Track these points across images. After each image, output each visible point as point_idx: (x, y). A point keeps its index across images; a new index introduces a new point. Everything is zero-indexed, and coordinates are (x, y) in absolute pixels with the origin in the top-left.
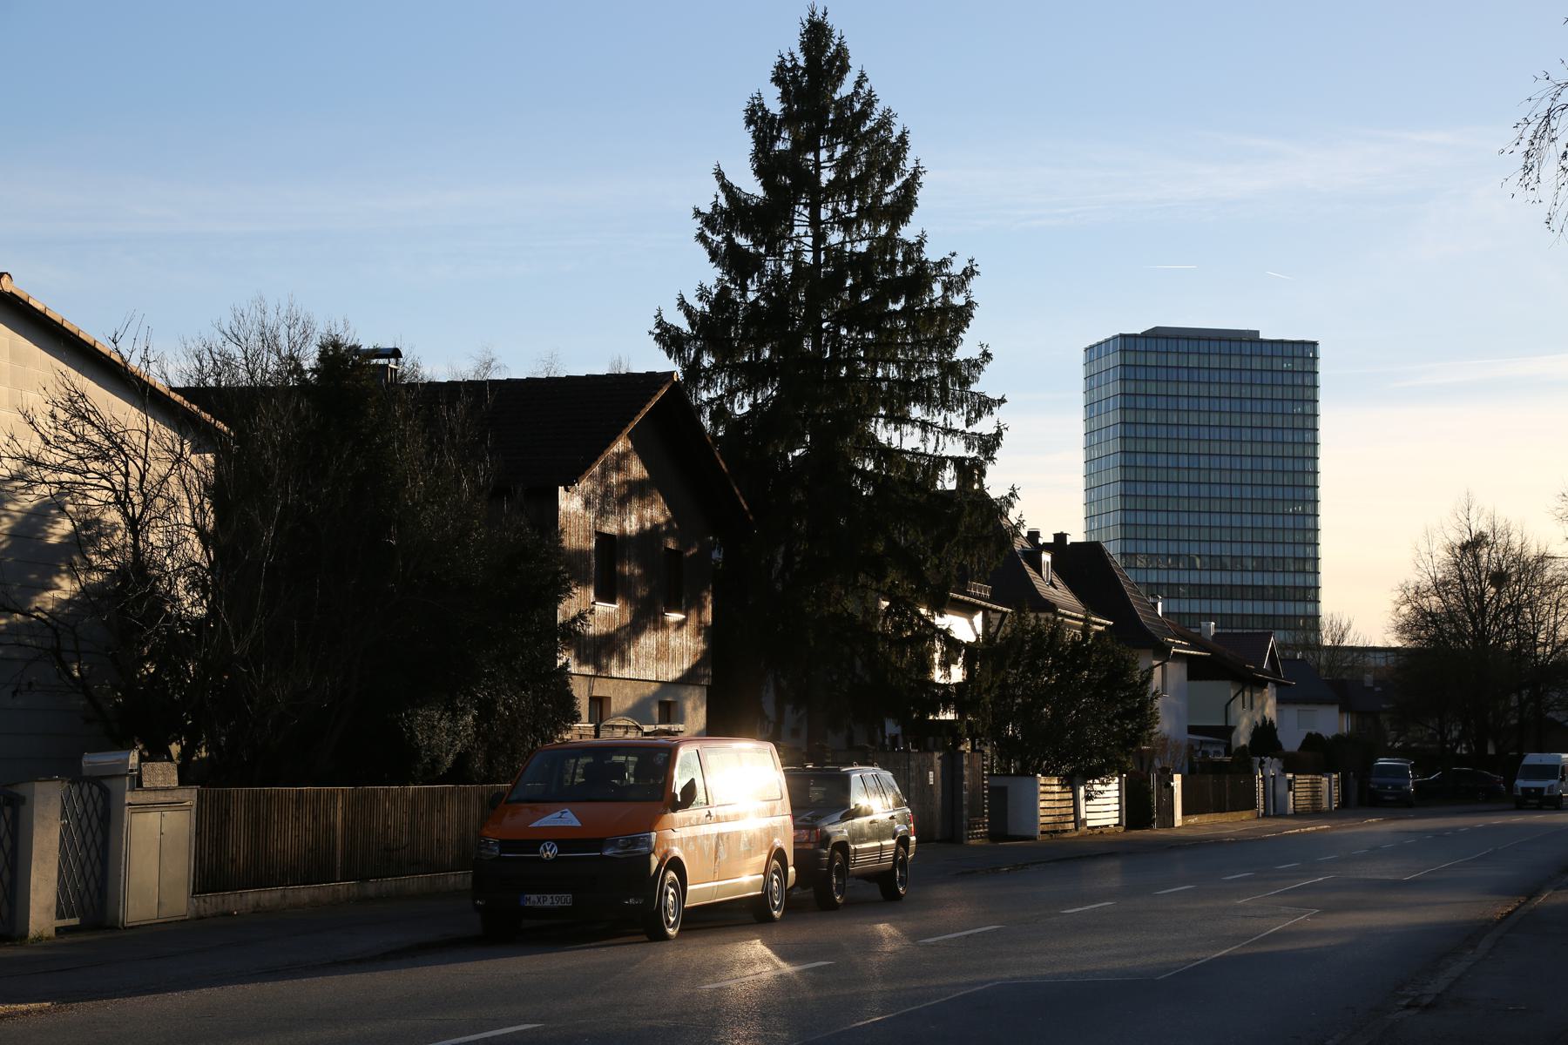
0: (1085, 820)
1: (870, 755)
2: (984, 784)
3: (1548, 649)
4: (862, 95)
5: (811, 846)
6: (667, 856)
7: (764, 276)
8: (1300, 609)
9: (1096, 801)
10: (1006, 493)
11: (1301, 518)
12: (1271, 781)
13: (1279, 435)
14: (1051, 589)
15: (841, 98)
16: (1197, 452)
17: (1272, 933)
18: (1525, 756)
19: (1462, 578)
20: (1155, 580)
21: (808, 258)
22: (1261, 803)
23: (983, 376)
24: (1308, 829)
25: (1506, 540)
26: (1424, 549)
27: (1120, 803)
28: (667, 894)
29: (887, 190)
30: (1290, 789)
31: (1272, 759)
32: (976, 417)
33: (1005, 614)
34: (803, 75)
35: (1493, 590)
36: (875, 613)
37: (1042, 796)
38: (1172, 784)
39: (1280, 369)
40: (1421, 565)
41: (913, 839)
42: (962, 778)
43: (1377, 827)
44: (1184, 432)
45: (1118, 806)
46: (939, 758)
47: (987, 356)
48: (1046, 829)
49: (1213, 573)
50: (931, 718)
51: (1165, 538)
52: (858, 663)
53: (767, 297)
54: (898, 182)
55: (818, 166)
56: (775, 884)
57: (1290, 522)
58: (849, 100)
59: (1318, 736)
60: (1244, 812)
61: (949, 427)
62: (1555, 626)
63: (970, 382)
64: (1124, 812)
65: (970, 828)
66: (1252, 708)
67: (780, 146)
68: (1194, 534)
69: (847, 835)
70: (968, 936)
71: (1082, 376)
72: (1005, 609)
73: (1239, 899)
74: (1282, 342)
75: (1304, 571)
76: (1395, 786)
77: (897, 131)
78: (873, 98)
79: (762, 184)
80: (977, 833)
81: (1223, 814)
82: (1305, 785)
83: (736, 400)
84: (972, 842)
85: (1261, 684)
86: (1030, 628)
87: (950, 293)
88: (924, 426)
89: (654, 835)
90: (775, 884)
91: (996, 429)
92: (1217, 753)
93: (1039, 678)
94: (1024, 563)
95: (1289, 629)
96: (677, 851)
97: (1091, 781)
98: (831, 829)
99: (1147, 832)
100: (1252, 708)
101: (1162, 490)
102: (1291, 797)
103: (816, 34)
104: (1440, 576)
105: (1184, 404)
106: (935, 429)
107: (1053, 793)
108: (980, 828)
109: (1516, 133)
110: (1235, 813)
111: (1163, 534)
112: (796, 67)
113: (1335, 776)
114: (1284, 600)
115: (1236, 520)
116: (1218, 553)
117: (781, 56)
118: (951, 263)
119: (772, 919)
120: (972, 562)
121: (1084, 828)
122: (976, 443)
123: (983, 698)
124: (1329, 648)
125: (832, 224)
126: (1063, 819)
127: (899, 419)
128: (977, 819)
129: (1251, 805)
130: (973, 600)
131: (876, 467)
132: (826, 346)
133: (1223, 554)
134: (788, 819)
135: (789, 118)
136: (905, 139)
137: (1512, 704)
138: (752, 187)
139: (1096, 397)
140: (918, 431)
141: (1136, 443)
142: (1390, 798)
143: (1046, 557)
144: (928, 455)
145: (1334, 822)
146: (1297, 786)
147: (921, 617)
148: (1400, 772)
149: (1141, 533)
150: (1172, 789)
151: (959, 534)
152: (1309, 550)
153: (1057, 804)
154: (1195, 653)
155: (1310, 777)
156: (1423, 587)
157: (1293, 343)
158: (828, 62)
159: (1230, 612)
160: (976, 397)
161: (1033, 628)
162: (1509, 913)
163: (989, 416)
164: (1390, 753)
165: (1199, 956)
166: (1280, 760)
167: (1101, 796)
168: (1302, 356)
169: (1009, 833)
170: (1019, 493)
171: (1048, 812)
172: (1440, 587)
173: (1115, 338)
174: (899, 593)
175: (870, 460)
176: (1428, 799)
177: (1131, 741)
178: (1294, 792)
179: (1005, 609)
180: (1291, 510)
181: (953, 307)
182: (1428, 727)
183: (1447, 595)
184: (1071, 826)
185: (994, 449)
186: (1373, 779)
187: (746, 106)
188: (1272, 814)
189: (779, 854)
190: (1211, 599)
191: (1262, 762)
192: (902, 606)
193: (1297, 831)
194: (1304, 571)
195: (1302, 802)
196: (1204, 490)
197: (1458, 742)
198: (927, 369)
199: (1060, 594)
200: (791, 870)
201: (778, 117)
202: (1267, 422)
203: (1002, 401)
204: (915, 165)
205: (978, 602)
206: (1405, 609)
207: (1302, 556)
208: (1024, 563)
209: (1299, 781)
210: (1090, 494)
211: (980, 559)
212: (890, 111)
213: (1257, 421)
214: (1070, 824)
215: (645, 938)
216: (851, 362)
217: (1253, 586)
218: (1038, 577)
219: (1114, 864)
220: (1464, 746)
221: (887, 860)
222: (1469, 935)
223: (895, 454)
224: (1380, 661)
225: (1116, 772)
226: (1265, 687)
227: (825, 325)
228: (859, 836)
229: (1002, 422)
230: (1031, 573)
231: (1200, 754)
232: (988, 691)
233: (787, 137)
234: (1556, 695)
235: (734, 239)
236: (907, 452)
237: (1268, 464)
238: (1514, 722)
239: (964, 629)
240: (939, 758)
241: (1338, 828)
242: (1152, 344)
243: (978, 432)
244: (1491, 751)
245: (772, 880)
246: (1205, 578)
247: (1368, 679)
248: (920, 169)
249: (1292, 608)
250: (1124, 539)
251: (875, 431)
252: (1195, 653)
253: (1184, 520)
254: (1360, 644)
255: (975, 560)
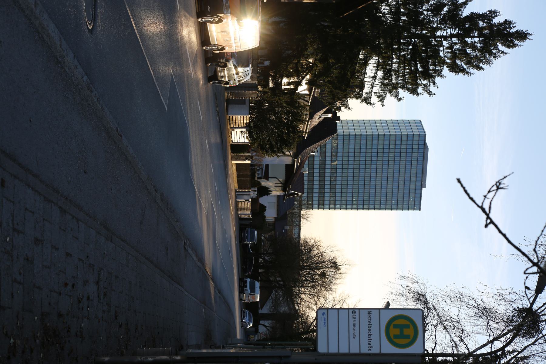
0: (234, 131)
1: (256, 61)
2: (246, 97)
3: (298, 291)
4: (499, 53)
5: (226, 56)
6: (223, 19)
7: (432, 17)
8: (316, 202)
9: (240, 134)
10: (350, 106)
11: (351, 203)
12: (249, 194)
13: (384, 195)
14: (318, 117)
15: (498, 45)
16: (378, 164)
17: (201, 203)
18: (259, 282)
19: (324, 262)
20: (327, 147)
21: (438, 33)
22: (241, 190)
23: (392, 98)
24: (231, 207)
25: (338, 278)
26: (335, 249)
27: (240, 142)
28: (211, 18)
29: (462, 63)
30: (245, 200)
31: (257, 194)
32: (377, 96)
33: (308, 102)
34: (507, 31)
35: (319, 273)
36: (308, 57)
37: (242, 117)
38: (247, 160)
39: (410, 196)
40: (329, 248)
41: (228, 86)
42: (249, 90)
43: (232, 230)
44: (386, 159)
45: (239, 142)
46: (255, 83)
47: (400, 100)
48: (230, 118)
49: (330, 169)
50: (270, 79)
51: (344, 151)
52: (290, 52)
53: (424, 18)
54: (465, 67)
55: (473, 37)
56: (214, 47)
57: (349, 199)
58: (497, 49)
59: (265, 210)
60: (237, 184)
61: (374, 86)
62: (306, 294)
63: (390, 93)
64: (237, 144)
65: (231, 93)
66: (275, 187)
67: (481, 23)
68: (345, 162)
69: (229, 67)
70: (199, 112)
71: (410, 119)
72: (310, 102)
73: (210, 190)
74: (421, 197)
75: (330, 204)
76: (247, 237)
77: (484, 66)
78: (496, 58)
79: (467, 16)
80: (229, 95)
81: (236, 177)
82: (247, 205)
83: (386, 7)
84: (226, 93)
85: (284, 190)
86: (302, 112)
87: (423, 86)
88: (375, 77)
89: (230, 15)
90: (214, 47)
91: (373, 103)
92: (259, 174)
93: (285, 115)
94: (328, 107)
95: (308, 198)
96: (224, 21)
97: (248, 133)
98: (231, 62)
99: (230, 151)
100: (275, 187)
101: (363, 150)
102: (243, 201)
103: (522, 36)
104: (325, 254)
105: (397, 159)
106: (373, 81)
107: (243, 120)
108: (231, 96)
109: (414, 274)
110: (237, 181)
111: (346, 150)
112: (510, 28)
113: (250, 216)
114: (319, 196)
115: (350, 179)
116: (337, 172)
117: (515, 23)
118: (435, 86)
119: (203, 46)
120: (325, 94)
121: (231, 130)
122: (368, 96)
123: (277, 98)
124: (300, 213)
125: (451, 43)
126: (234, 123)
127: (378, 66)
128: (234, 95)
129: (240, 187)
130: (313, 91)
131: (360, 59)
132: (405, 40)
133: (337, 173)
134: (235, 51)
135: (491, 26)
136: (481, 69)
137: (277, 278)
138: (466, 12)
139: (401, 124)
140: (373, 75)
141: (382, 140)
142: (243, 235)
143: (330, 115)
144: (364, 78)
145: (234, 216)
146: (247, 203)
147: (306, 75)
148: (252, 239)
149: (346, 142)
150: (245, 160)
151: (335, 90)
152: (338, 206)
153: (239, 122)
154: (295, 167)
155: (250, 207)
156: (321, 248)
157: (420, 201)
158: (512, 40)
159: (314, 176)
160: (385, 96)
161: (302, 113)
162: (207, 272)
163: (378, 101)
164: (259, 235)
165: (195, 182)
166: (256, 197)
167: (243, 136)
168: (416, 205)
169: (229, 105)
170: (350, 111)
171: (237, 119)
172: (321, 254)
173: (425, 132)
174: (315, 68)
175: (363, 57)
176: (243, 248)
177: (263, 148)
178: (245, 202)
179: (310, 102)
180: (354, 199)
181: (417, 88)
182: (269, 249)
183: (318, 256)
184: (232, 126)
185: (366, 102)
186: (249, 229)
187: (497, 10)
188: (237, 194)
189: (223, 49)
190: (320, 168)
191: (255, 191)
192: (310, 69)
193: (231, 203)
194: (330, 204)
195: (241, 204)
196: (362, 167)
197: (263, 259)
198: (395, 78)
199: (316, 120)
200: (218, 52)
201: (492, 22)
202: (389, 191)
203: (383, 105)
204: (471, 73)
205: (312, 93)
206: (313, 242)
207: (336, 203)
208: (328, 107)
209: (248, 204)
210: (362, 122)
211: (326, 96)
212: (492, 64)
213: (389, 187)
214: (232, 126)
215: (197, 12)
216: (399, 50)
217: (324, 185)
218: (323, 112)
219: (219, 140)
220: (262, 261)
221: (221, 78)
222: (201, 259)
223: (365, 66)
224: (295, 232)
225: (251, 142)
226: (283, 191)
227: (413, 40)
228: (229, 70)
229: (375, 105)
230: (324, 110)
231: (258, 168)
232: (279, 99)
233: (484, 25)
234: (281, 293)
235: (446, 7)
236: (365, 71)
237: (372, 191)
238: (271, 279)
239: (303, 89)
240: (255, 83)
241: (232, 217)
242: (421, 147)
243: (372, 97)
244: (260, 271)
245: (215, 46)
246: (328, 166)
247: (287, 228)
248: (470, 75)
249: (316, 199)
250: (344, 135)
251: (373, 59)
252: (295, 167)
253: (351, 159)
254: (301, 225)
255: (326, 95)
